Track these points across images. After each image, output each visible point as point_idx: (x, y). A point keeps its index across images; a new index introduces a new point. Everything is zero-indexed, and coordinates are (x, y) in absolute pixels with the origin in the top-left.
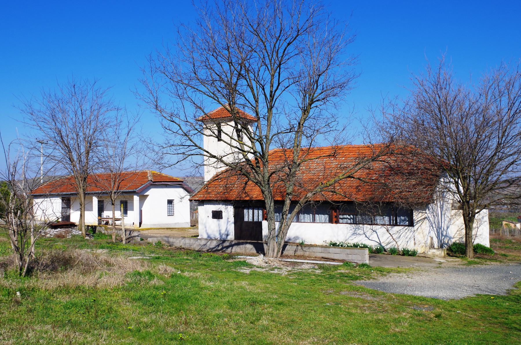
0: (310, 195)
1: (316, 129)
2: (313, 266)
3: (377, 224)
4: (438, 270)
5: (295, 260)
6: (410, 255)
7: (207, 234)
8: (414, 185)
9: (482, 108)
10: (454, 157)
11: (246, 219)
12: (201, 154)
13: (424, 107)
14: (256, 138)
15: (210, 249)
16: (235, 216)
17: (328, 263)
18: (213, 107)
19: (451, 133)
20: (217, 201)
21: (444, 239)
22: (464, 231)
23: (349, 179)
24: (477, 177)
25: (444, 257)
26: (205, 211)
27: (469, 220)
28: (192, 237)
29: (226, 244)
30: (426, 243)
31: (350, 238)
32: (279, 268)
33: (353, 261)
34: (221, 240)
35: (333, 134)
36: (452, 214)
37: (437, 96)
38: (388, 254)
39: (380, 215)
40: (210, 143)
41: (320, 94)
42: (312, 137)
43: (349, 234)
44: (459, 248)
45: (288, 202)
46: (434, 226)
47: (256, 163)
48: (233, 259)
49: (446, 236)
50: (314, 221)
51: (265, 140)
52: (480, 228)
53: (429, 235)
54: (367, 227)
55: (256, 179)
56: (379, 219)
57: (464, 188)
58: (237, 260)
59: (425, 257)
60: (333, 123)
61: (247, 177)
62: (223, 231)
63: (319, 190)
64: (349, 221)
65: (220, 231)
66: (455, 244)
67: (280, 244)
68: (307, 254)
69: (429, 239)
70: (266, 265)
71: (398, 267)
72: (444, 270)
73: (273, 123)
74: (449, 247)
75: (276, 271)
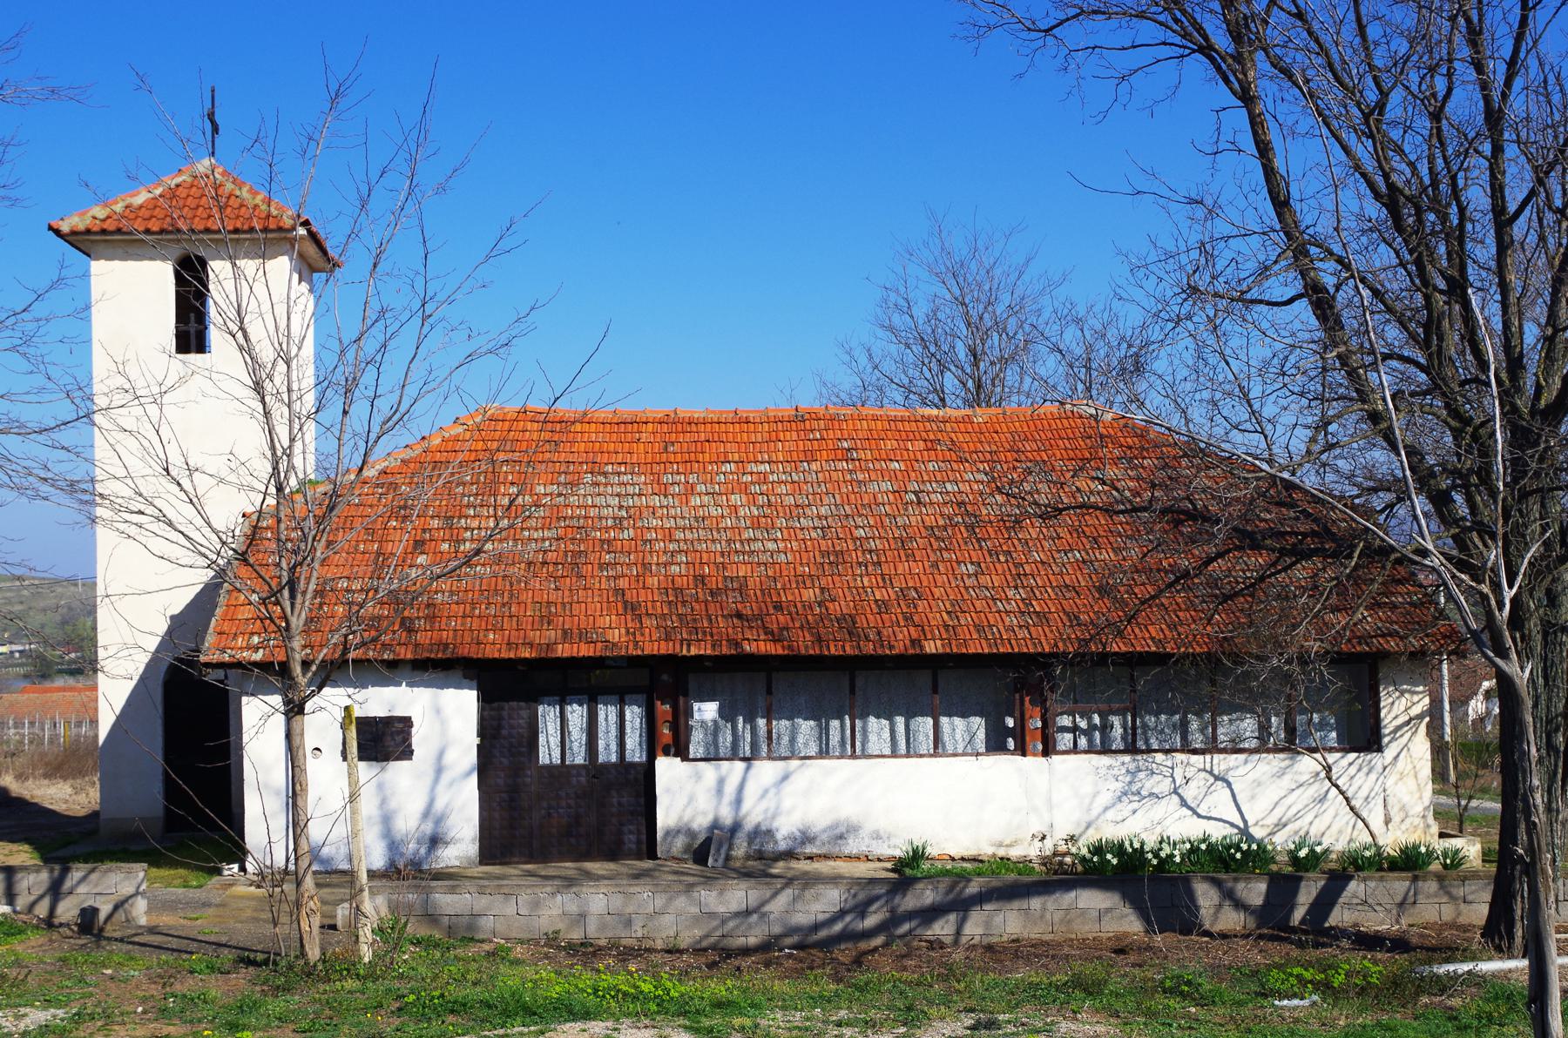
20: (393, 665)
31: (1110, 815)
43: (1105, 798)
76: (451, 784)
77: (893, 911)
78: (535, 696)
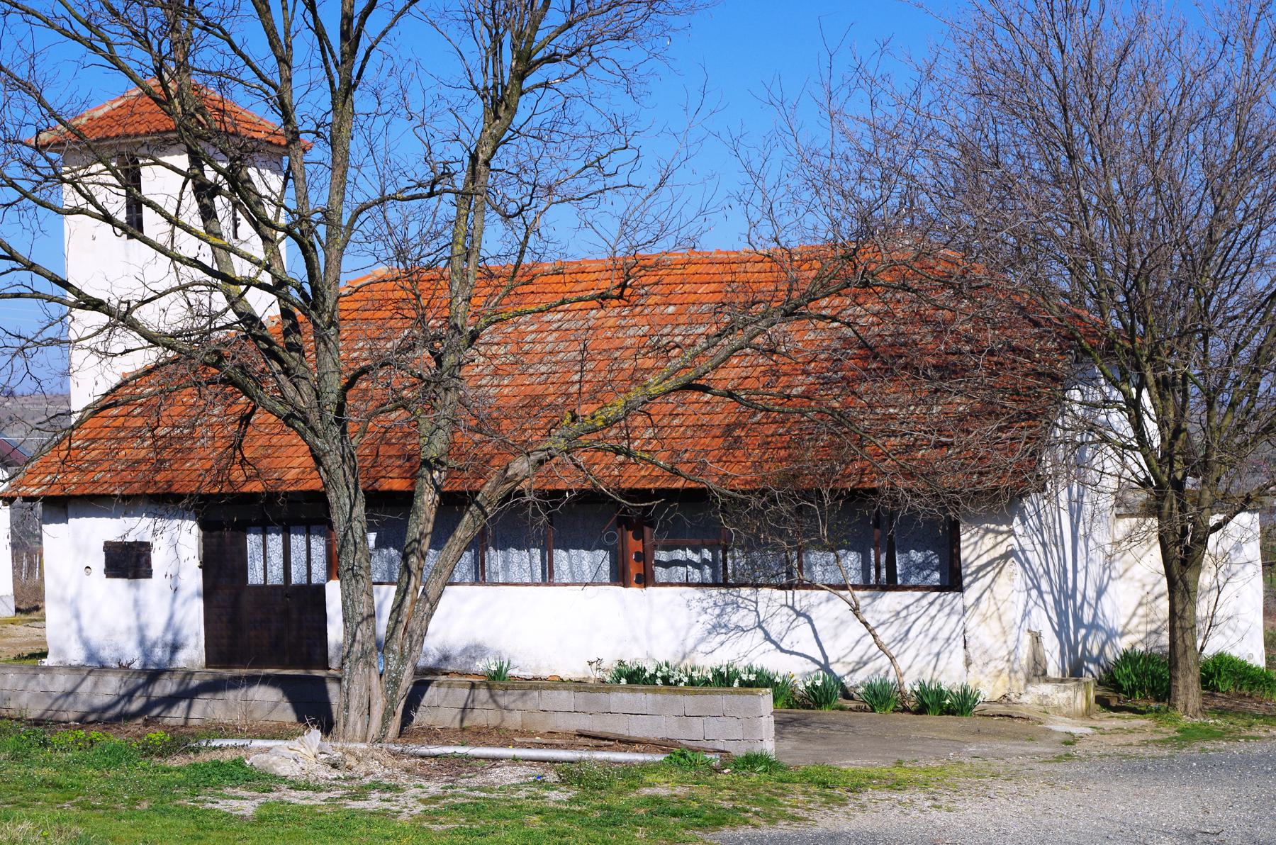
0: (520, 466)
1: (542, 181)
2: (539, 770)
3: (811, 586)
4: (1060, 768)
5: (461, 750)
6: (949, 711)
7: (86, 643)
8: (962, 418)
9: (1231, 95)
10: (1121, 298)
11: (255, 576)
12: (36, 295)
13: (998, 88)
14: (283, 221)
15: (94, 711)
16: (208, 564)
17: (600, 755)
18: (97, 91)
19: (1108, 199)
21: (1085, 638)
22: (1164, 604)
23: (695, 396)
24: (1213, 380)
25: (1087, 714)
26: (75, 545)
27: (1182, 560)
28: (20, 658)
29: (166, 687)
30: (1011, 657)
31: (703, 647)
32: (388, 788)
33: (709, 745)
34: (143, 670)
35: (618, 203)
36: (1119, 537)
37: (1053, 43)
38: (858, 709)
39: (824, 548)
40: (96, 257)
41: (562, 30)
42: (530, 215)
43: (698, 630)
44: (1144, 674)
45: (427, 500)
46: (1045, 586)
47: (286, 333)
48: (186, 752)
49: (1094, 626)
50: (548, 577)
51: (322, 230)
52: (1228, 590)
53: (1025, 625)
54: (771, 599)
55: (284, 400)
56: (819, 564)
57: (1162, 425)
58: (204, 757)
59: (1008, 719)
60: (618, 158)
61: (246, 393)
62: (155, 631)
63: (562, 444)
64: (696, 576)
65: (141, 629)
66: (1128, 658)
67: (396, 683)
68: (514, 720)
69: (1026, 640)
70: (336, 773)
71: (899, 763)
72: (1082, 769)
73: (357, 147)
74: (1107, 671)
75: (374, 802)
76: (184, 603)
77: (149, 697)
78: (244, 528)
